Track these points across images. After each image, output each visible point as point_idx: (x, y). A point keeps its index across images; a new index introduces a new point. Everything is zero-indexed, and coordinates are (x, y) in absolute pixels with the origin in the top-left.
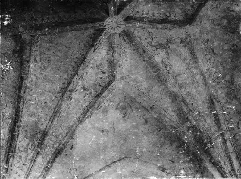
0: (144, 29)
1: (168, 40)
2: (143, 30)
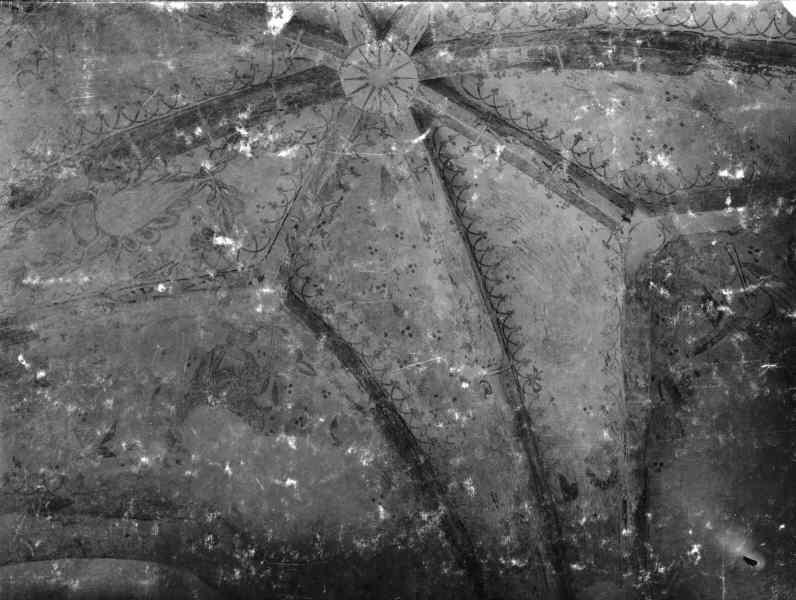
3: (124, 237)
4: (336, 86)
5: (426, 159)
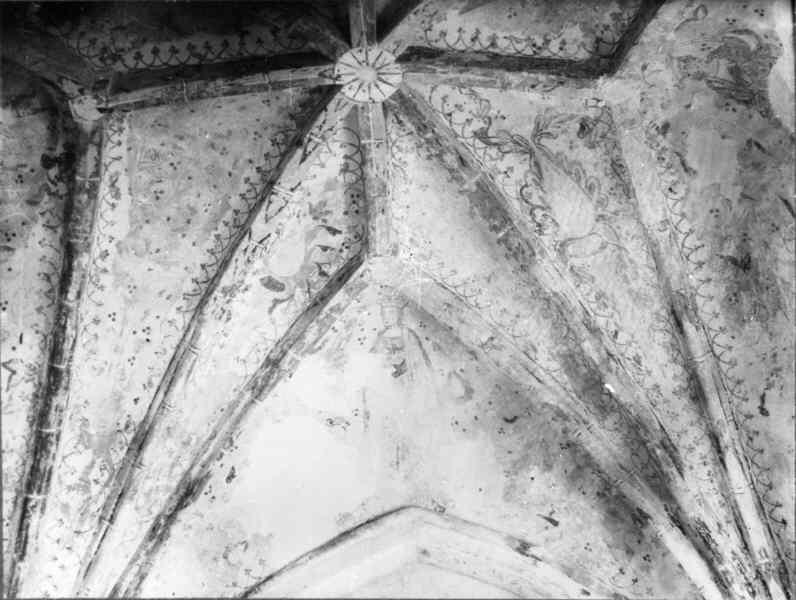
1: (541, 126)
2: (461, 93)
3: (596, 209)
4: (394, 99)
5: (415, 13)
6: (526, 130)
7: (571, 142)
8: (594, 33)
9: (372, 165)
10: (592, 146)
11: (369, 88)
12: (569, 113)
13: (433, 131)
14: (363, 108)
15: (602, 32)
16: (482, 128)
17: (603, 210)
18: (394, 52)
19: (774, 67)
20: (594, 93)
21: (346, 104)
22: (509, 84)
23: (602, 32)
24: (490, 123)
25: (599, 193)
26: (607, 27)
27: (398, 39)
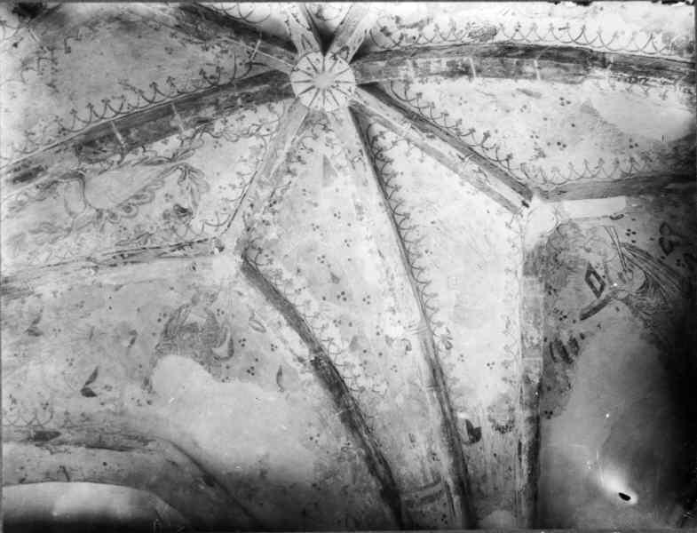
0: (256, 128)
1: (193, 174)
2: (253, 125)
4: (287, 88)
5: (361, 151)
6: (193, 161)
7: (171, 197)
8: (268, 248)
9: (231, 38)
10: (166, 216)
11: (309, 75)
12: (201, 204)
13: (241, 107)
14: (293, 59)
15: (267, 256)
16: (213, 130)
17: (106, 218)
18: (333, 114)
19: (199, 366)
20: (230, 250)
21: (304, 48)
22: (262, 187)
23: (267, 256)
24: (214, 137)
25: (122, 216)
26: (271, 261)
27: (344, 123)
